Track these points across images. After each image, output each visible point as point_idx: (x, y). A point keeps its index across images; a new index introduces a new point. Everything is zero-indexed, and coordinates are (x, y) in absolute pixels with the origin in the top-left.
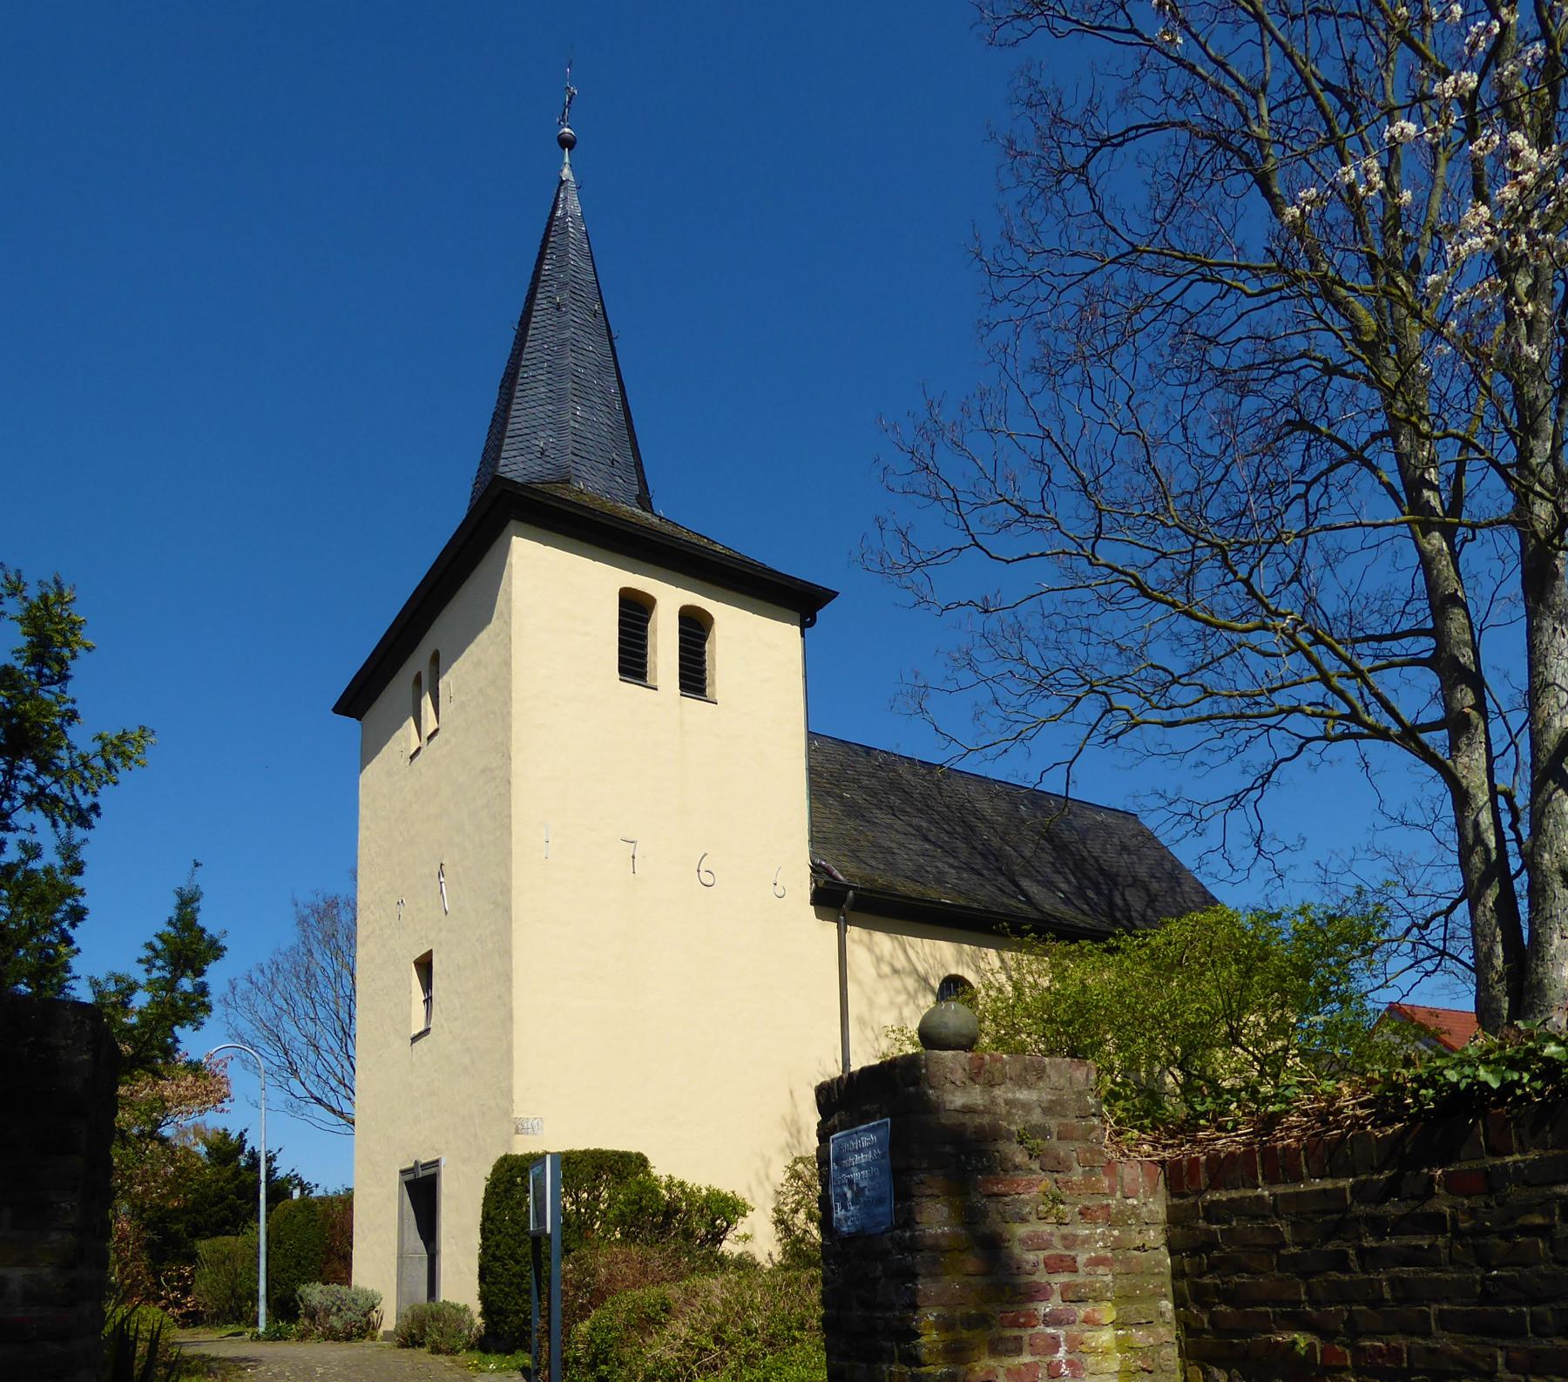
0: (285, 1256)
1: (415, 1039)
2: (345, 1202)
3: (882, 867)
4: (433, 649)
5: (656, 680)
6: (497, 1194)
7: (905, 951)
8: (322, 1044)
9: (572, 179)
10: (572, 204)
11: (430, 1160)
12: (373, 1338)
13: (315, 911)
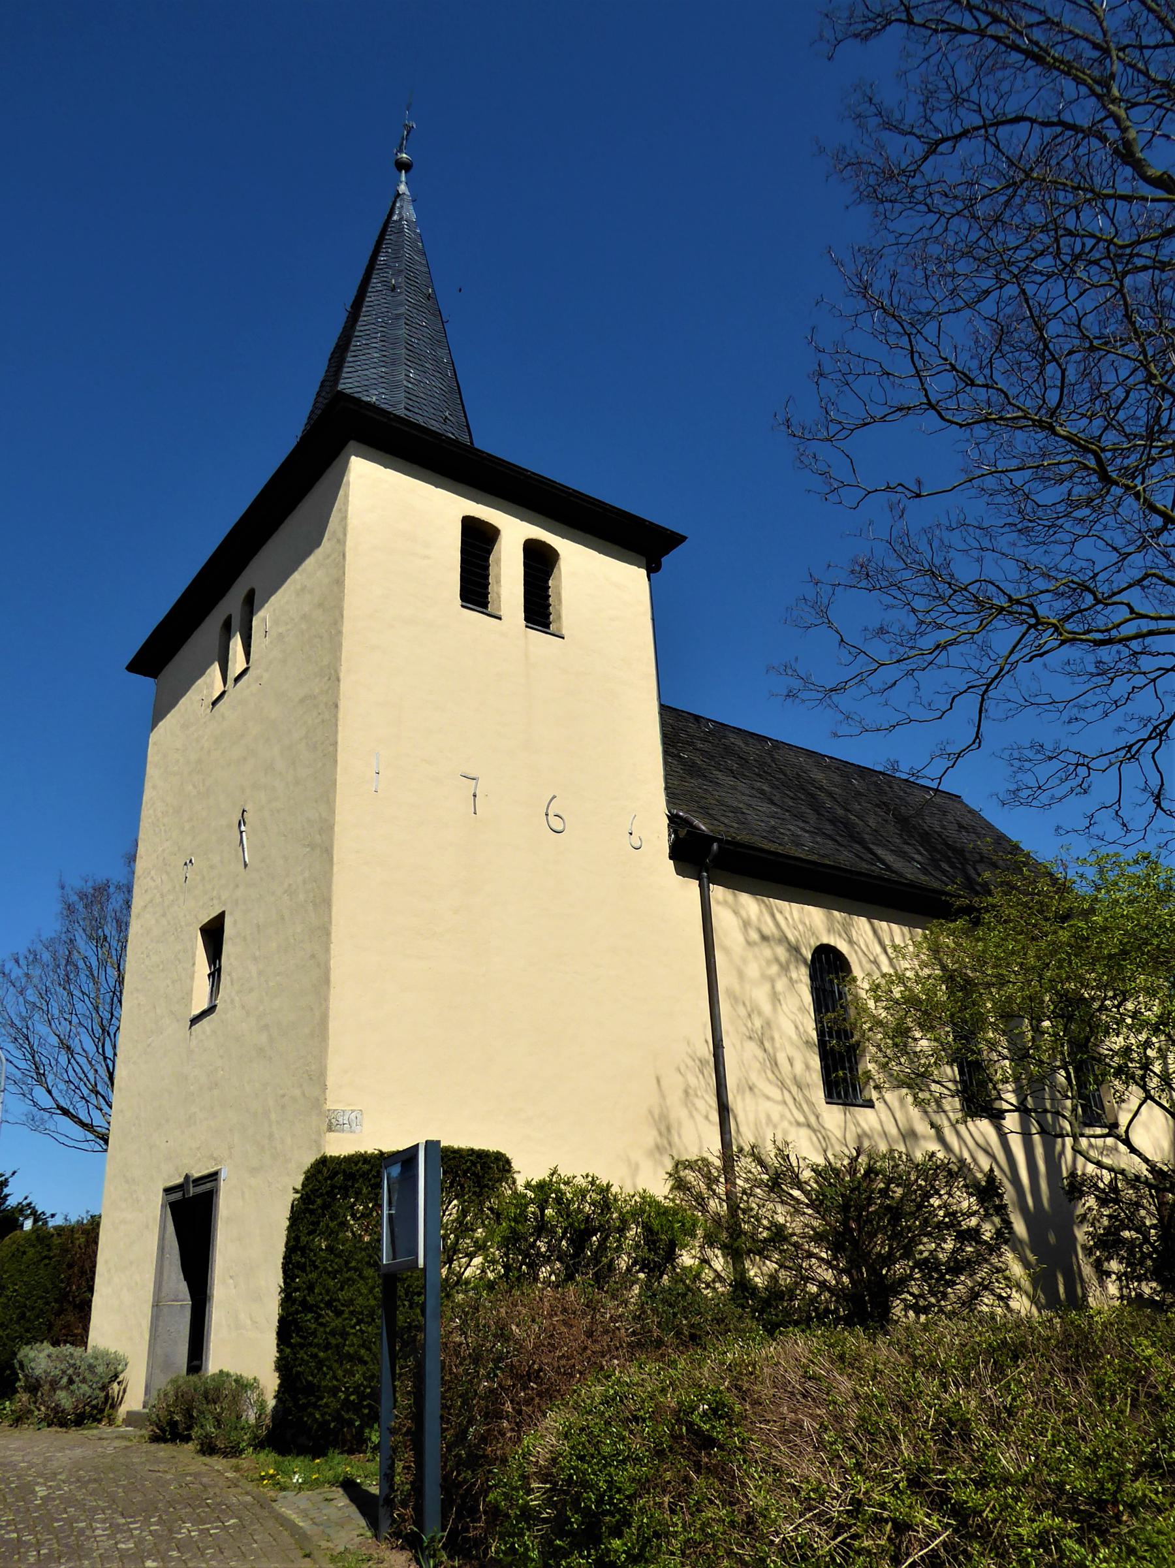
1: (195, 1020)
2: (90, 1231)
3: (736, 825)
5: (499, 609)
6: (312, 1212)
7: (773, 916)
8: (75, 1044)
9: (408, 193)
10: (407, 212)
11: (205, 1172)
12: (111, 1422)
13: (82, 896)
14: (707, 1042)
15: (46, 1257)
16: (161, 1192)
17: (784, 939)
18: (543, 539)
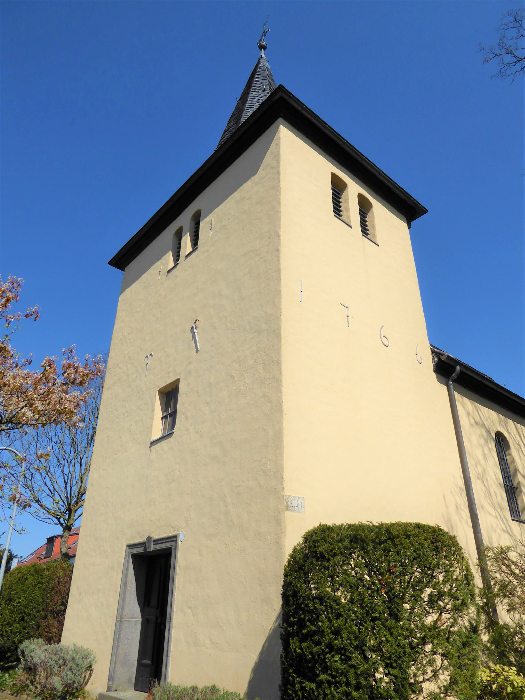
0: (12, 612)
4: (180, 226)
11: (171, 534)
14: (461, 477)
15: (39, 583)
16: (125, 547)
17: (484, 426)
18: (366, 196)
